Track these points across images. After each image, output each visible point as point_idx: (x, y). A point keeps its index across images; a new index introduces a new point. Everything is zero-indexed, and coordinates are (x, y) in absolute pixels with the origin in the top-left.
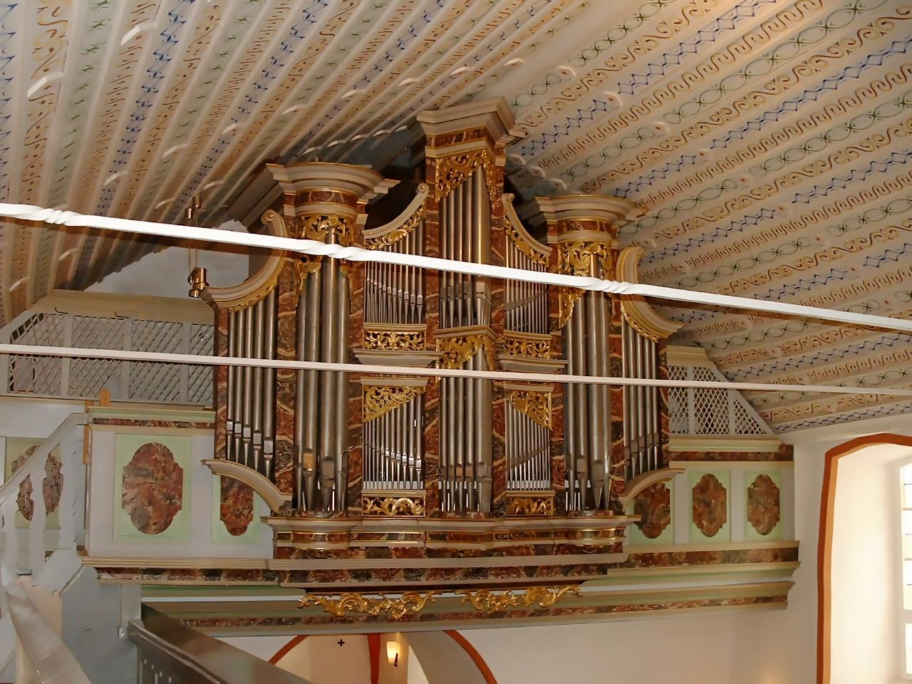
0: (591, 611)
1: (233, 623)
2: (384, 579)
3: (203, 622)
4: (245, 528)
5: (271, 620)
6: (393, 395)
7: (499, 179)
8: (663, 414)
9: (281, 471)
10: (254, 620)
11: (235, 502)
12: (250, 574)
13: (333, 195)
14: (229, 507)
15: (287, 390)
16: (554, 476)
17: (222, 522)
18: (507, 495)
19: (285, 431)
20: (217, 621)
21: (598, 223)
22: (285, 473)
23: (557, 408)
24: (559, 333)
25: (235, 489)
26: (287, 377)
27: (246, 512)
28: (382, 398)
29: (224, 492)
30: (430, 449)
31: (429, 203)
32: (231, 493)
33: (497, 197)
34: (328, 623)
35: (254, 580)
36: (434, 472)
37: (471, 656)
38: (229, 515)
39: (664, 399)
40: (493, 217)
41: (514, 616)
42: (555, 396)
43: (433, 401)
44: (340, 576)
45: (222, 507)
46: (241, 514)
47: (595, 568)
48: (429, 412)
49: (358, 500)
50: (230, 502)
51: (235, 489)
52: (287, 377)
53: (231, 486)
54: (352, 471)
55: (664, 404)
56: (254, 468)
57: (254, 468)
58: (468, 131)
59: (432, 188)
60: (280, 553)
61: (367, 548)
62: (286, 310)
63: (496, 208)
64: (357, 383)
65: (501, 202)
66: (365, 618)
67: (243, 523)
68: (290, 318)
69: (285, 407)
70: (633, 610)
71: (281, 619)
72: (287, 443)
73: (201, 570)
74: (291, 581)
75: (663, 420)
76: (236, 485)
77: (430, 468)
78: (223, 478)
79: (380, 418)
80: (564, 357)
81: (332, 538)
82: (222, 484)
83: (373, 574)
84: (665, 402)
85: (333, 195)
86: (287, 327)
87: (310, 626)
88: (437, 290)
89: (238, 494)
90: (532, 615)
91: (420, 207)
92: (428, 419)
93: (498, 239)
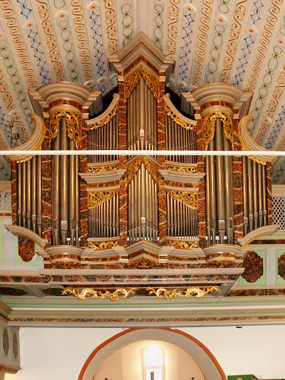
0: (255, 318)
1: (59, 320)
2: (103, 281)
3: (45, 319)
4: (31, 259)
5: (79, 320)
6: (105, 196)
7: (162, 88)
8: (268, 200)
9: (45, 231)
10: (70, 319)
11: (26, 247)
12: (36, 280)
13: (63, 101)
14: (23, 250)
15: (48, 196)
16: (199, 232)
17: (19, 256)
18: (167, 239)
19: (47, 214)
20: (52, 319)
21: (220, 102)
22: (47, 232)
23: (201, 199)
24: (203, 163)
25: (25, 242)
26: (47, 190)
27: (31, 252)
28: (99, 197)
29: (20, 244)
30: (122, 218)
31: (120, 103)
32: (24, 243)
33: (161, 97)
34: (108, 321)
35: (38, 282)
36: (124, 228)
37: (203, 349)
38: (23, 253)
39: (269, 192)
40: (158, 107)
41: (210, 320)
42: (199, 193)
43: (123, 195)
44: (79, 279)
45: (19, 250)
46: (29, 252)
47: (227, 277)
48: (122, 201)
49: (86, 244)
50: (23, 247)
51: (25, 242)
52: (47, 190)
53: (23, 240)
54: (82, 231)
55: (269, 195)
56: (33, 231)
57: (33, 231)
58: (135, 61)
59: (122, 96)
60: (46, 266)
61: (91, 265)
62: (46, 160)
63: (160, 102)
64: (85, 191)
65: (163, 99)
66: (127, 320)
67: (30, 256)
68: (49, 163)
69: (46, 203)
70: (281, 318)
71: (83, 319)
72: (48, 219)
73: (11, 277)
74: (54, 281)
75: (269, 203)
76: (26, 240)
77: (122, 227)
78: (19, 238)
79: (98, 207)
80: (205, 172)
81: (72, 256)
82: (19, 240)
83: (97, 279)
84: (270, 194)
85: (63, 101)
86: (46, 167)
87: (98, 322)
88: (126, 143)
89: (27, 244)
90: (220, 320)
91: (116, 106)
92: (121, 204)
93: (161, 117)
